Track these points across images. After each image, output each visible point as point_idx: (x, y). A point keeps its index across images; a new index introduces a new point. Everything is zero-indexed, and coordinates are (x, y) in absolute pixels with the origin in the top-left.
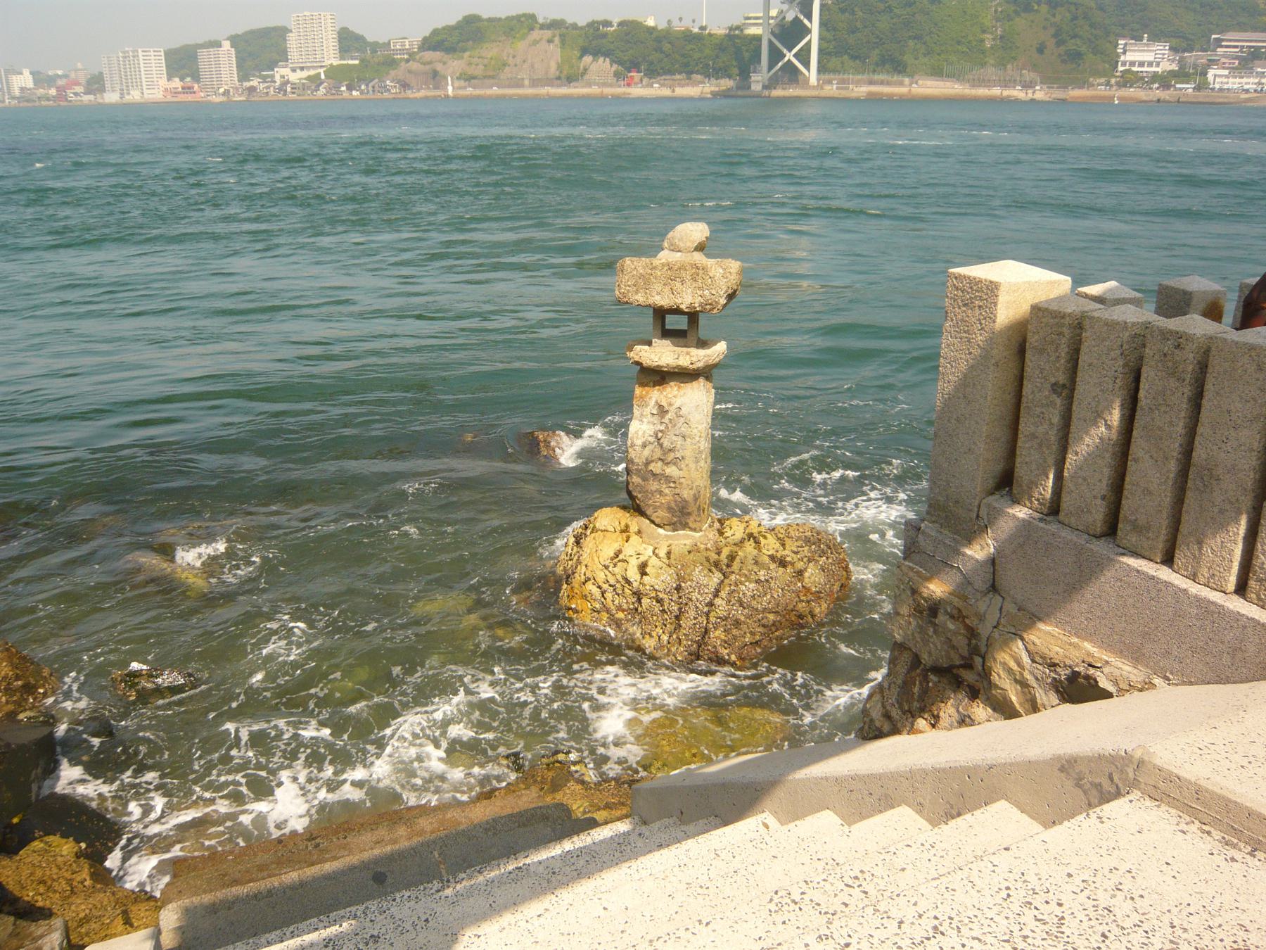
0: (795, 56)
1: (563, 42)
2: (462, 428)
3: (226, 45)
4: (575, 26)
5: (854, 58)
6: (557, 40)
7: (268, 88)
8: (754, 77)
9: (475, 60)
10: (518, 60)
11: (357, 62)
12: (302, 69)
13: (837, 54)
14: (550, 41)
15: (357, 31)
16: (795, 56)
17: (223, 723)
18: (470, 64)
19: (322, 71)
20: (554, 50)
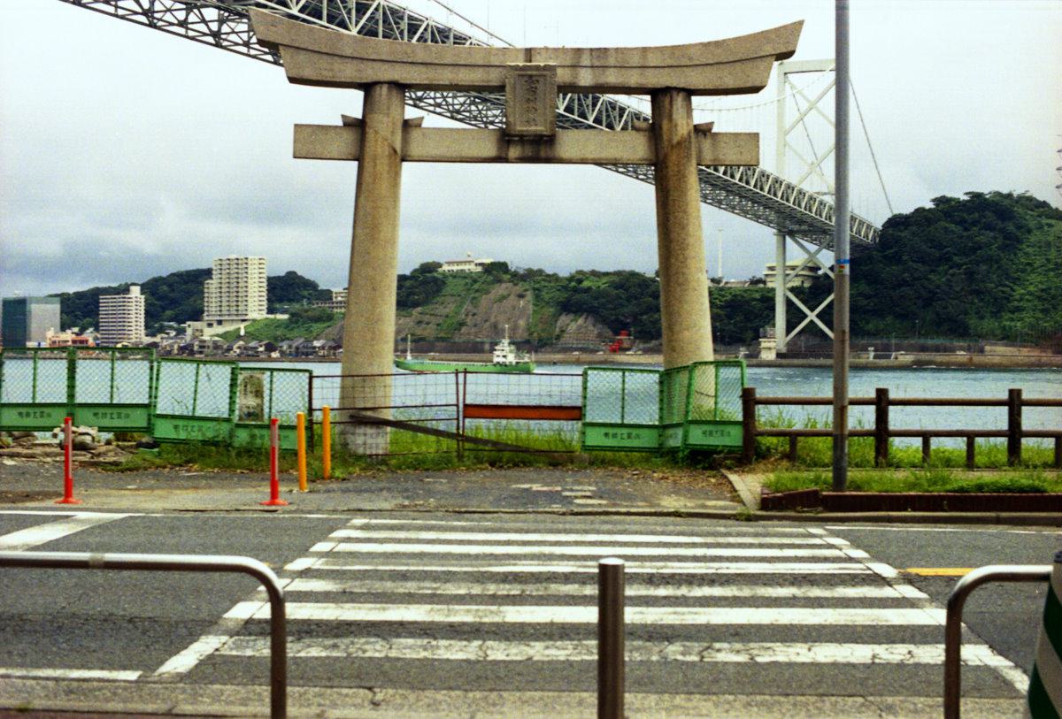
0: (806, 316)
1: (537, 297)
2: (210, 704)
3: (135, 291)
4: (555, 277)
5: (903, 317)
6: (529, 295)
7: (171, 346)
8: (764, 343)
9: (426, 318)
10: (478, 319)
11: (286, 317)
12: (220, 322)
13: (878, 313)
14: (521, 296)
15: (307, 276)
16: (806, 316)
17: (836, 295)
18: (420, 322)
19: (242, 326)
20: (527, 304)
